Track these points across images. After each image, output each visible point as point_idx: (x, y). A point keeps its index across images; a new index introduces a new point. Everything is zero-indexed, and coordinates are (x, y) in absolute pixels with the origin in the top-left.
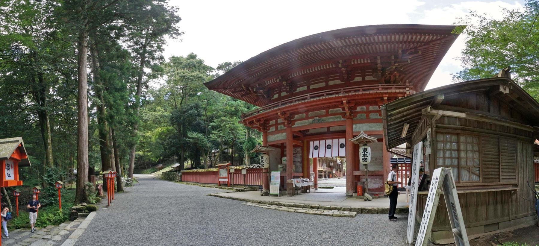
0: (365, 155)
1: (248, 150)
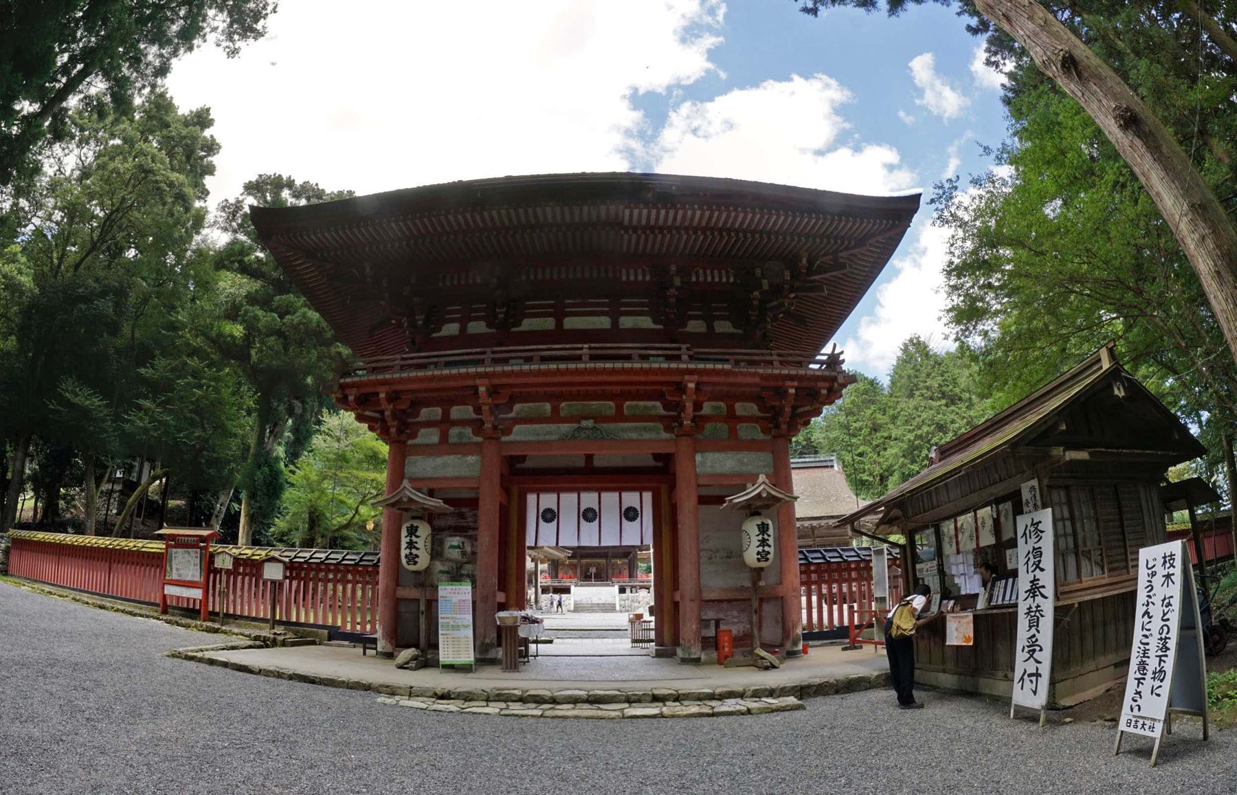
0: (411, 545)
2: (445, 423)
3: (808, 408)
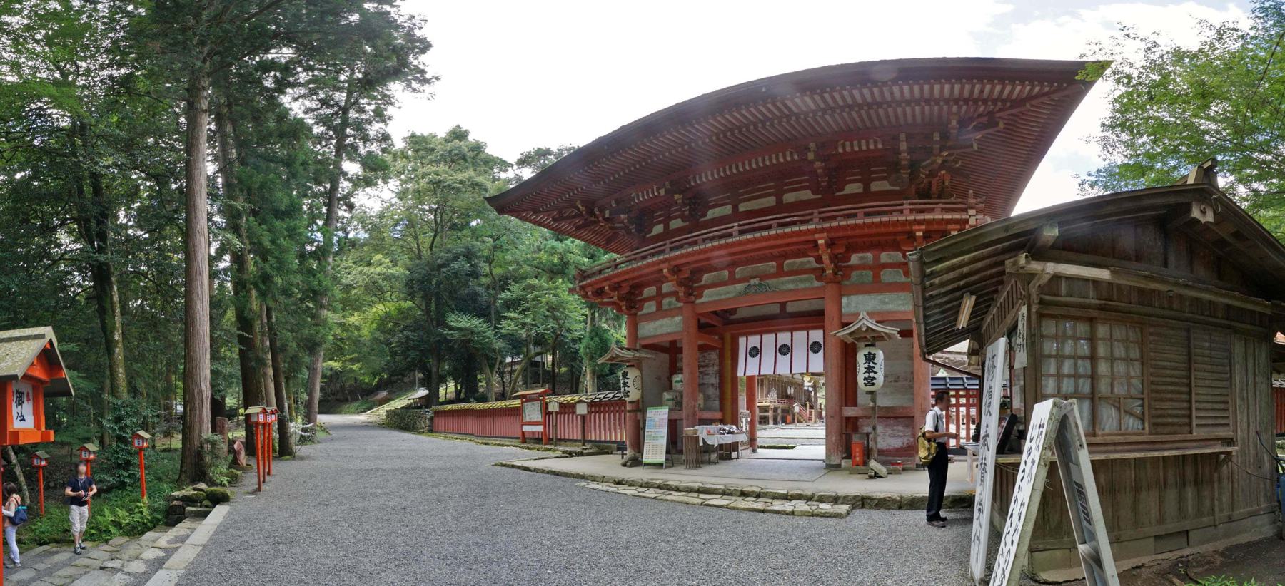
0: (869, 369)
1: (592, 358)
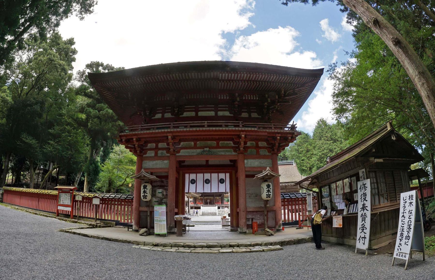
0: (145, 192)
2: (157, 149)
3: (284, 144)
